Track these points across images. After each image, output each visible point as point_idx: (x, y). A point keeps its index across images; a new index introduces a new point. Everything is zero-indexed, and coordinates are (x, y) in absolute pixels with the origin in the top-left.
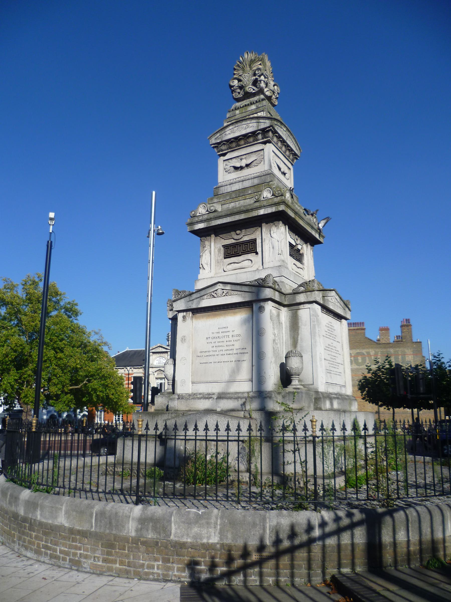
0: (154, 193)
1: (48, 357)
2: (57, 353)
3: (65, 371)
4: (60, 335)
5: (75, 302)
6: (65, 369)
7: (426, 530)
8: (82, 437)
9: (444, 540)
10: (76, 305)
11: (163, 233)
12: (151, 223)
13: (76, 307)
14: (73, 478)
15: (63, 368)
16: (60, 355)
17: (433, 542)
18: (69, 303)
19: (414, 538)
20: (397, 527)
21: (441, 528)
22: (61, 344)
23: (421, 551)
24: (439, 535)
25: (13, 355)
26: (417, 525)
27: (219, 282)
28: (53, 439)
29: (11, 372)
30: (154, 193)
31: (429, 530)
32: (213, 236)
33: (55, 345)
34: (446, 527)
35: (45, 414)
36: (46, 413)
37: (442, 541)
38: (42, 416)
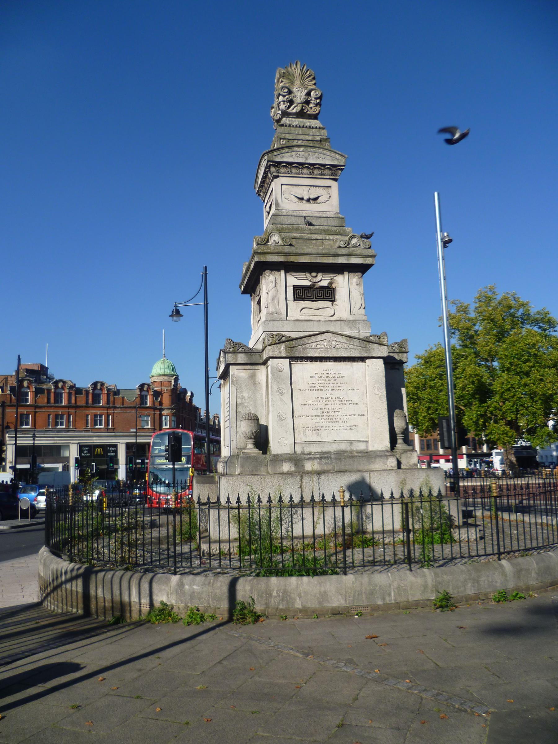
0: (436, 194)
1: (512, 385)
2: (521, 378)
3: (536, 399)
4: (523, 355)
5: (546, 311)
6: (536, 396)
7: (116, 592)
8: (485, 483)
9: (130, 602)
10: (547, 313)
11: (450, 241)
12: (437, 232)
13: (548, 316)
14: (545, 531)
15: (532, 395)
16: (526, 380)
17: (122, 604)
18: (538, 313)
19: (108, 597)
20: (98, 584)
21: (127, 593)
22: (525, 367)
23: (113, 607)
24: (126, 599)
25: (470, 388)
26: (110, 586)
27: (327, 332)
28: (548, 482)
29: (473, 407)
30: (436, 194)
31: (118, 592)
32: (346, 273)
33: (518, 369)
34: (131, 593)
35: (554, 450)
36: (555, 448)
37: (128, 604)
38: (551, 453)
